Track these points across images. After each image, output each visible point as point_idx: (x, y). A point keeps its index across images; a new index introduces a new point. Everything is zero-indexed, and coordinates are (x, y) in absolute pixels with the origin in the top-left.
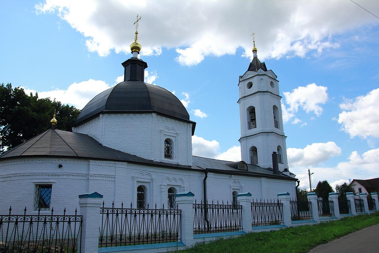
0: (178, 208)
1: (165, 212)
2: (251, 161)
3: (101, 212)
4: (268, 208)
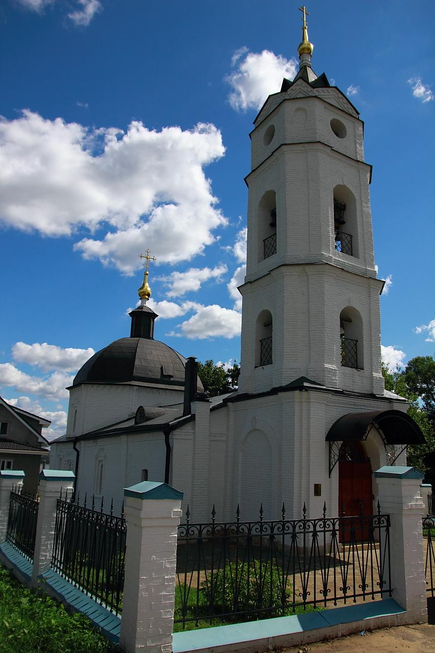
0: (379, 512)
1: (309, 526)
2: (260, 352)
3: (257, 530)
4: (195, 497)
